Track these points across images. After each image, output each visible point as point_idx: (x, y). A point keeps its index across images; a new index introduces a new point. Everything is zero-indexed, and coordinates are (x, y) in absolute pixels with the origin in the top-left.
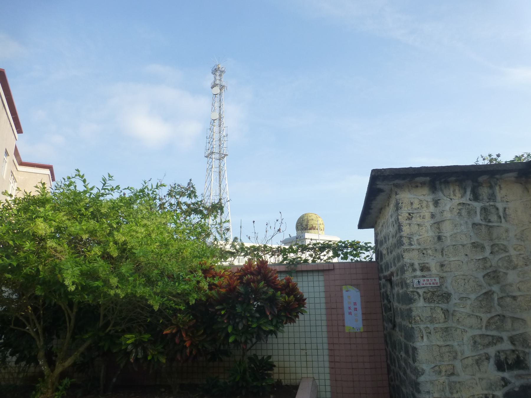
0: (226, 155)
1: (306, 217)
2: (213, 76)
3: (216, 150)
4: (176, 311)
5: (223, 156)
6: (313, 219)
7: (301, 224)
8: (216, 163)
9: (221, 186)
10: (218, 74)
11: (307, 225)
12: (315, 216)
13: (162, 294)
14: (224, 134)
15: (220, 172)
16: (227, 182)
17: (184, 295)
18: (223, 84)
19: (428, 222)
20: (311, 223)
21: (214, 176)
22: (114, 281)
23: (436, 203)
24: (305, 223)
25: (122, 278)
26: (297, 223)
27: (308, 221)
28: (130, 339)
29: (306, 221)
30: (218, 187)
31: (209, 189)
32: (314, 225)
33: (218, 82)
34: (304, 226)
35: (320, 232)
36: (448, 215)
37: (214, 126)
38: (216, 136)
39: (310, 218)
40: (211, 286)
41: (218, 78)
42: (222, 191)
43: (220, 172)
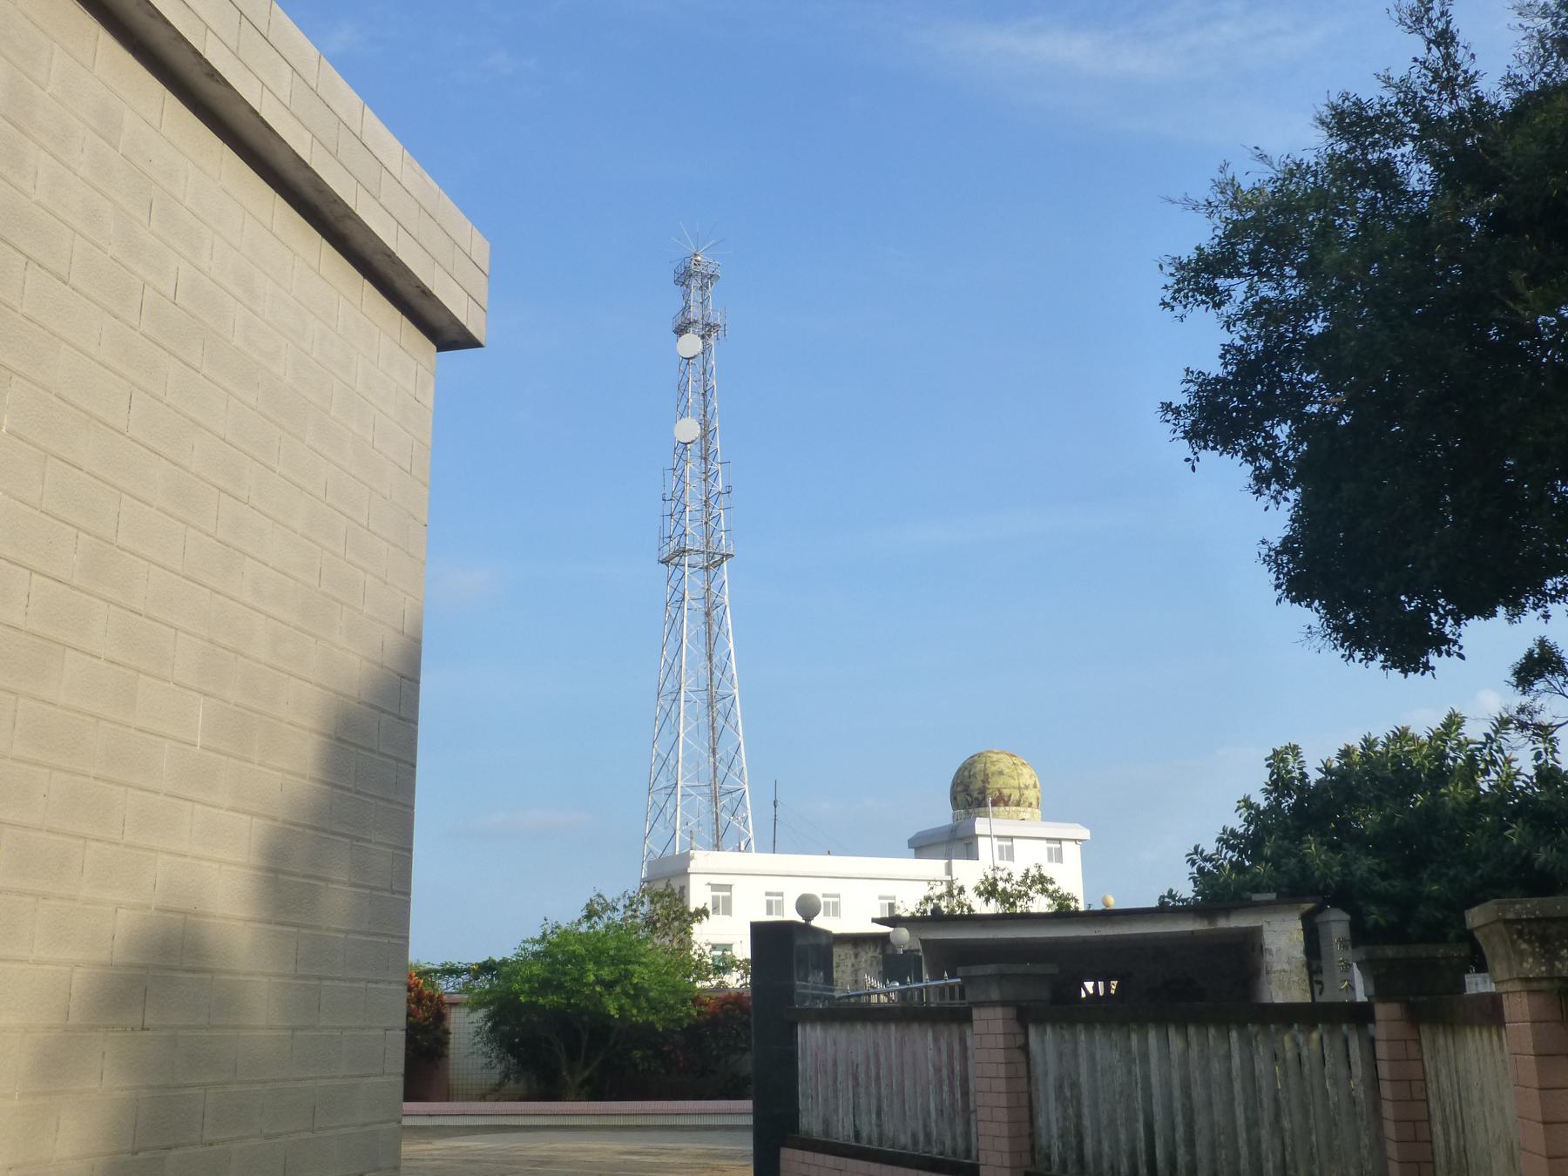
0: (728, 556)
1: (980, 766)
2: (679, 289)
3: (694, 541)
4: (673, 1032)
5: (717, 558)
6: (1001, 773)
7: (966, 789)
8: (693, 583)
9: (715, 660)
10: (695, 283)
11: (983, 791)
12: (1010, 761)
13: (664, 1019)
14: (720, 487)
15: (708, 614)
16: (731, 645)
17: (680, 1019)
18: (711, 321)
19: (849, 969)
20: (996, 783)
21: (690, 627)
22: (635, 1011)
23: (856, 956)
24: (979, 784)
25: (640, 1010)
26: (955, 785)
27: (986, 781)
28: (637, 1054)
29: (980, 778)
30: (704, 662)
31: (676, 669)
32: (1006, 792)
33: (696, 312)
34: (975, 794)
35: (1025, 812)
36: (863, 965)
37: (686, 461)
38: (693, 493)
39: (994, 769)
40: (699, 1013)
41: (695, 295)
42: (717, 674)
43: (708, 614)
